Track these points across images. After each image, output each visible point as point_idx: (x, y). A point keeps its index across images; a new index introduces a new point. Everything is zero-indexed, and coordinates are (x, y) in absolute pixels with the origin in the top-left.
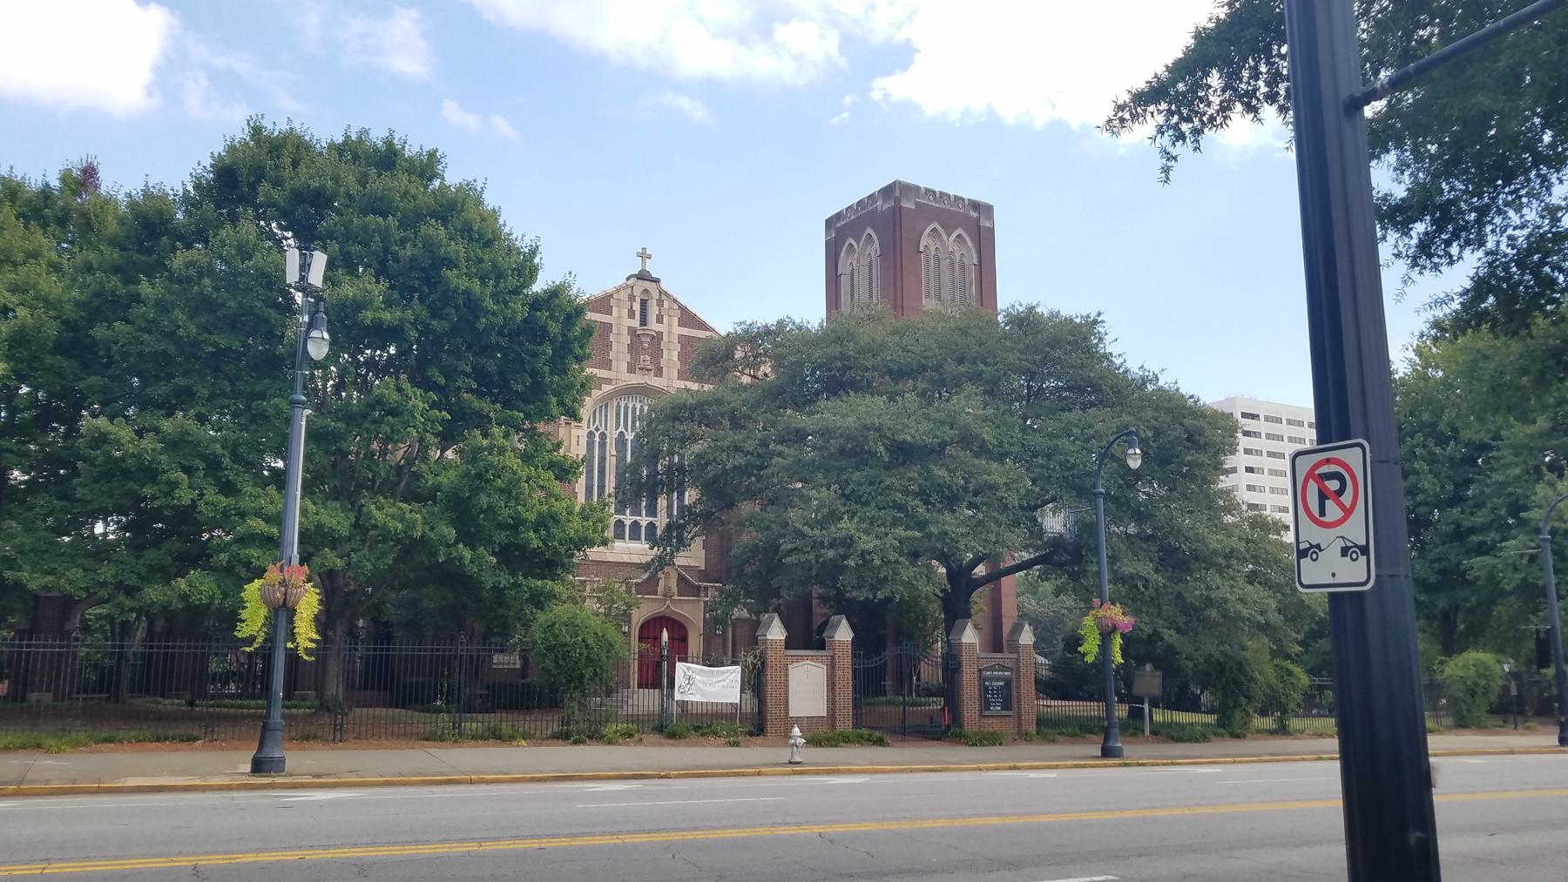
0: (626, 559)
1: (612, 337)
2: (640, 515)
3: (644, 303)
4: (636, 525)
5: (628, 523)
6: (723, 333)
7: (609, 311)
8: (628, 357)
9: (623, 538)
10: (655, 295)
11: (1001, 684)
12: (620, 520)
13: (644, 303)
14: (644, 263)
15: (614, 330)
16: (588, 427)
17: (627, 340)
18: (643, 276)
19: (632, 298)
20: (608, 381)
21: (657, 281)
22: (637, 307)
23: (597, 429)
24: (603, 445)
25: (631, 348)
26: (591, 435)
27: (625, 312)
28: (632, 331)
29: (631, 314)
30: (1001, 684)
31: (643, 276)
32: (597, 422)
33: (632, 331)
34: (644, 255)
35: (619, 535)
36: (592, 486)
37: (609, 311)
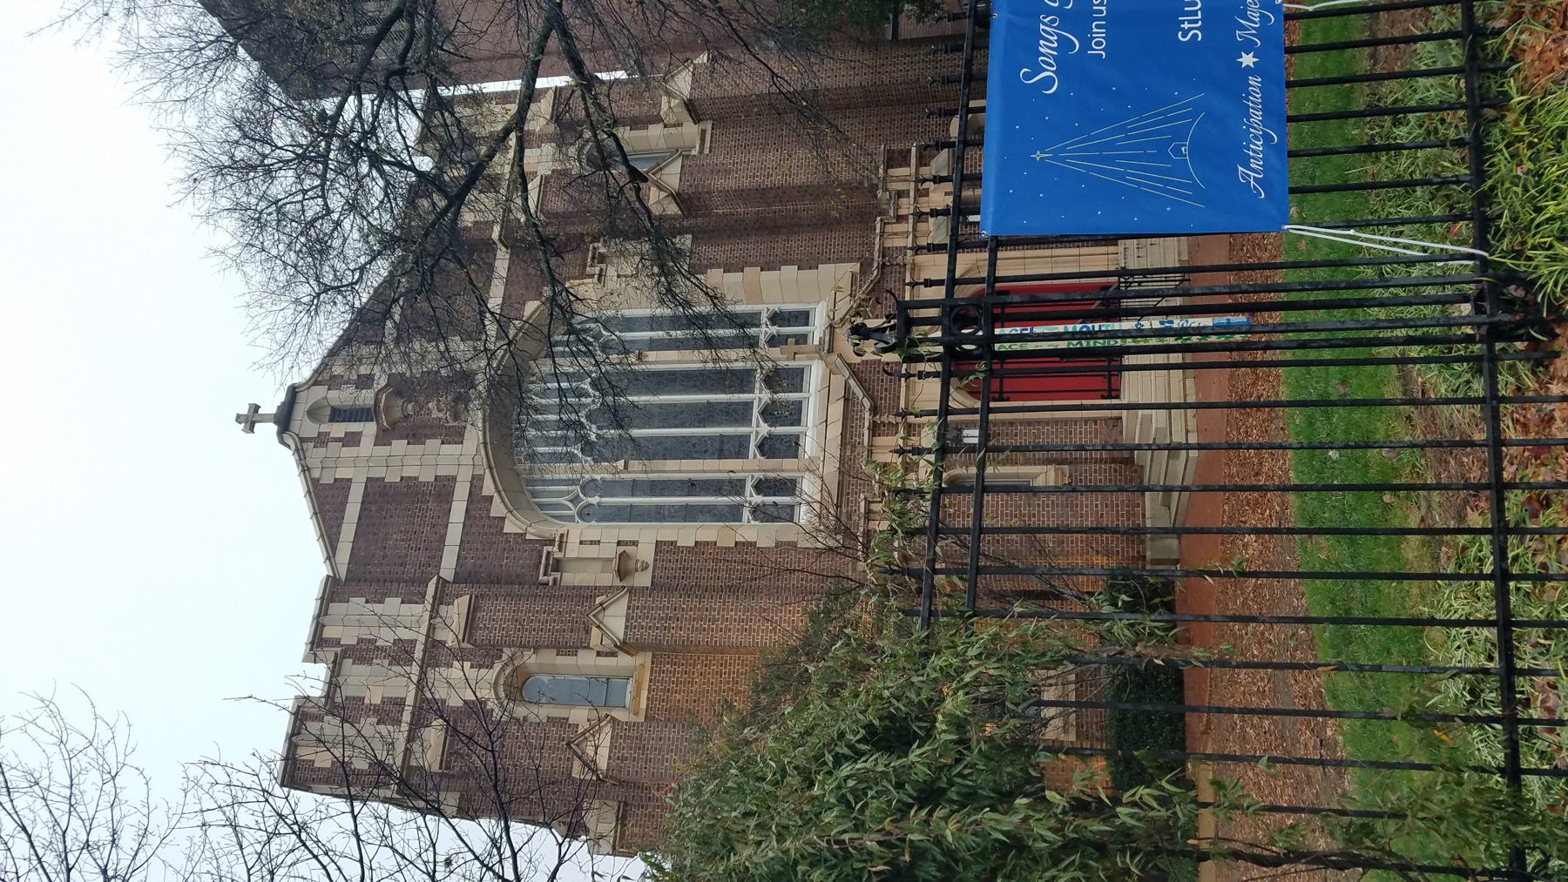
0: (835, 430)
1: (393, 477)
2: (748, 406)
3: (338, 415)
4: (769, 414)
5: (765, 429)
6: (935, 441)
7: (344, 485)
8: (433, 444)
9: (798, 437)
10: (319, 392)
11: (1539, 300)
12: (761, 447)
13: (338, 415)
14: (264, 419)
15: (377, 473)
16: (571, 519)
17: (399, 446)
18: (284, 419)
19: (322, 440)
20: (476, 482)
21: (293, 392)
22: (339, 429)
23: (575, 500)
24: (607, 488)
25: (415, 437)
26: (586, 514)
27: (348, 452)
28: (383, 438)
29: (352, 440)
30: (1539, 300)
31: (284, 419)
32: (562, 500)
33: (383, 438)
34: (250, 420)
35: (791, 447)
36: (659, 507)
37: (344, 485)
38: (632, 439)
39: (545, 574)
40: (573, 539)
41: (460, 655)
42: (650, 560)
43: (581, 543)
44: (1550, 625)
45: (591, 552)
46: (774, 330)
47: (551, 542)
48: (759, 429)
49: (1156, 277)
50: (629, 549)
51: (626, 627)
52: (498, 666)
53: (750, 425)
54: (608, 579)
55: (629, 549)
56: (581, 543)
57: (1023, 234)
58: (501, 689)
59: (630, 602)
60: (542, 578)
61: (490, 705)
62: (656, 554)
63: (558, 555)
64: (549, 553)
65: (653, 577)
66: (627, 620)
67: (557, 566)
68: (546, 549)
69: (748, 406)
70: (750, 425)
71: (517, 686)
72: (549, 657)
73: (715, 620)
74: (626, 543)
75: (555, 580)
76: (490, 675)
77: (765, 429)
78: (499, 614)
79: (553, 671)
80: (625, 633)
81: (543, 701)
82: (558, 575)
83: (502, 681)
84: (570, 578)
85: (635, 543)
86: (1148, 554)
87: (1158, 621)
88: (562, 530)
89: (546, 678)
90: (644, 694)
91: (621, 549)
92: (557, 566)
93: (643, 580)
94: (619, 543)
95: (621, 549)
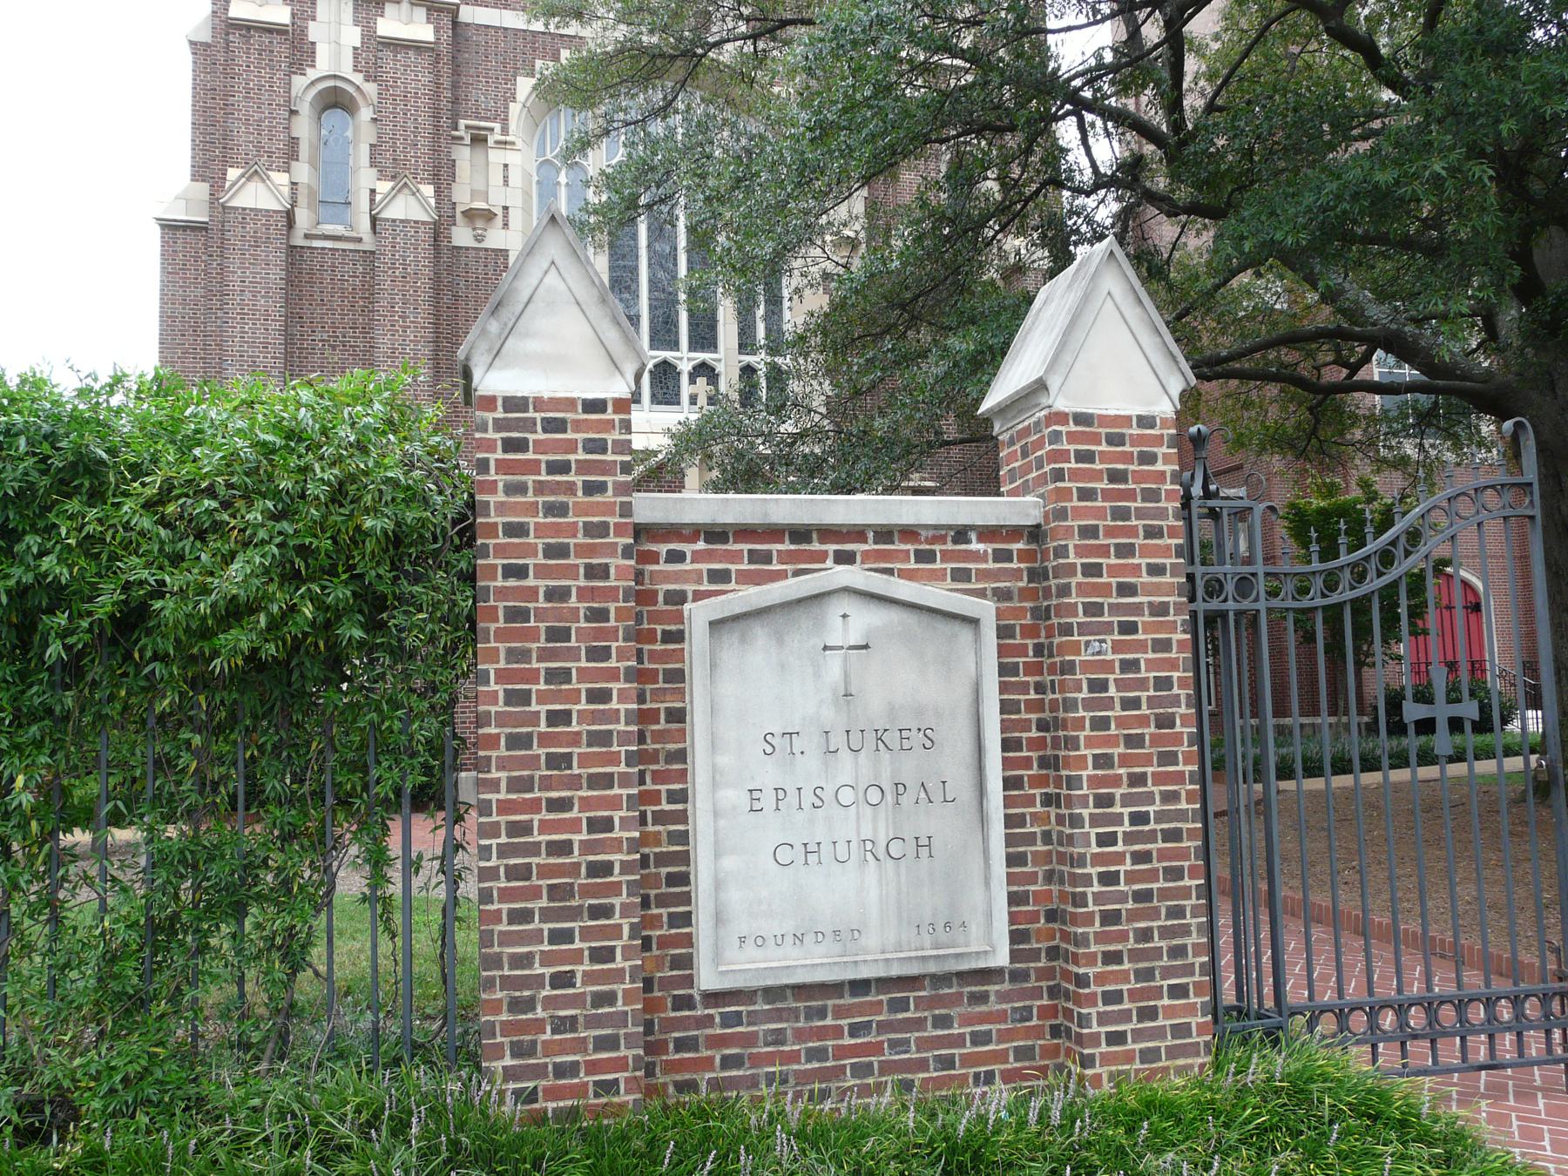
2: (675, 345)
5: (685, 367)
38: (633, 220)
39: (467, 127)
40: (511, 157)
41: (369, 34)
42: (486, 244)
43: (506, 166)
44: (4, 1086)
45: (496, 177)
46: (762, 370)
47: (505, 131)
48: (685, 359)
49: (1260, 836)
50: (499, 221)
51: (394, 221)
52: (358, 79)
53: (690, 349)
54: (462, 196)
55: (499, 221)
56: (506, 166)
57: (738, 610)
58: (331, 83)
59: (423, 223)
60: (462, 123)
61: (309, 71)
62: (493, 250)
63: (490, 142)
64: (492, 130)
65: (467, 249)
66: (402, 221)
67: (479, 140)
68: (497, 126)
69: (675, 345)
70: (690, 349)
71: (335, 100)
72: (368, 135)
73: (403, 317)
74: (506, 216)
75: (461, 138)
76: (347, 70)
77: (685, 367)
78: (417, 78)
79: (356, 141)
80: (236, 208)
81: (324, 132)
82: (468, 141)
83: (340, 84)
84: (463, 155)
85: (506, 225)
86: (463, 774)
87: (1211, 929)
88: (519, 144)
89: (349, 134)
90: (328, 244)
91: (499, 211)
92: (479, 140)
93: (462, 236)
94: (506, 208)
95: (499, 211)
